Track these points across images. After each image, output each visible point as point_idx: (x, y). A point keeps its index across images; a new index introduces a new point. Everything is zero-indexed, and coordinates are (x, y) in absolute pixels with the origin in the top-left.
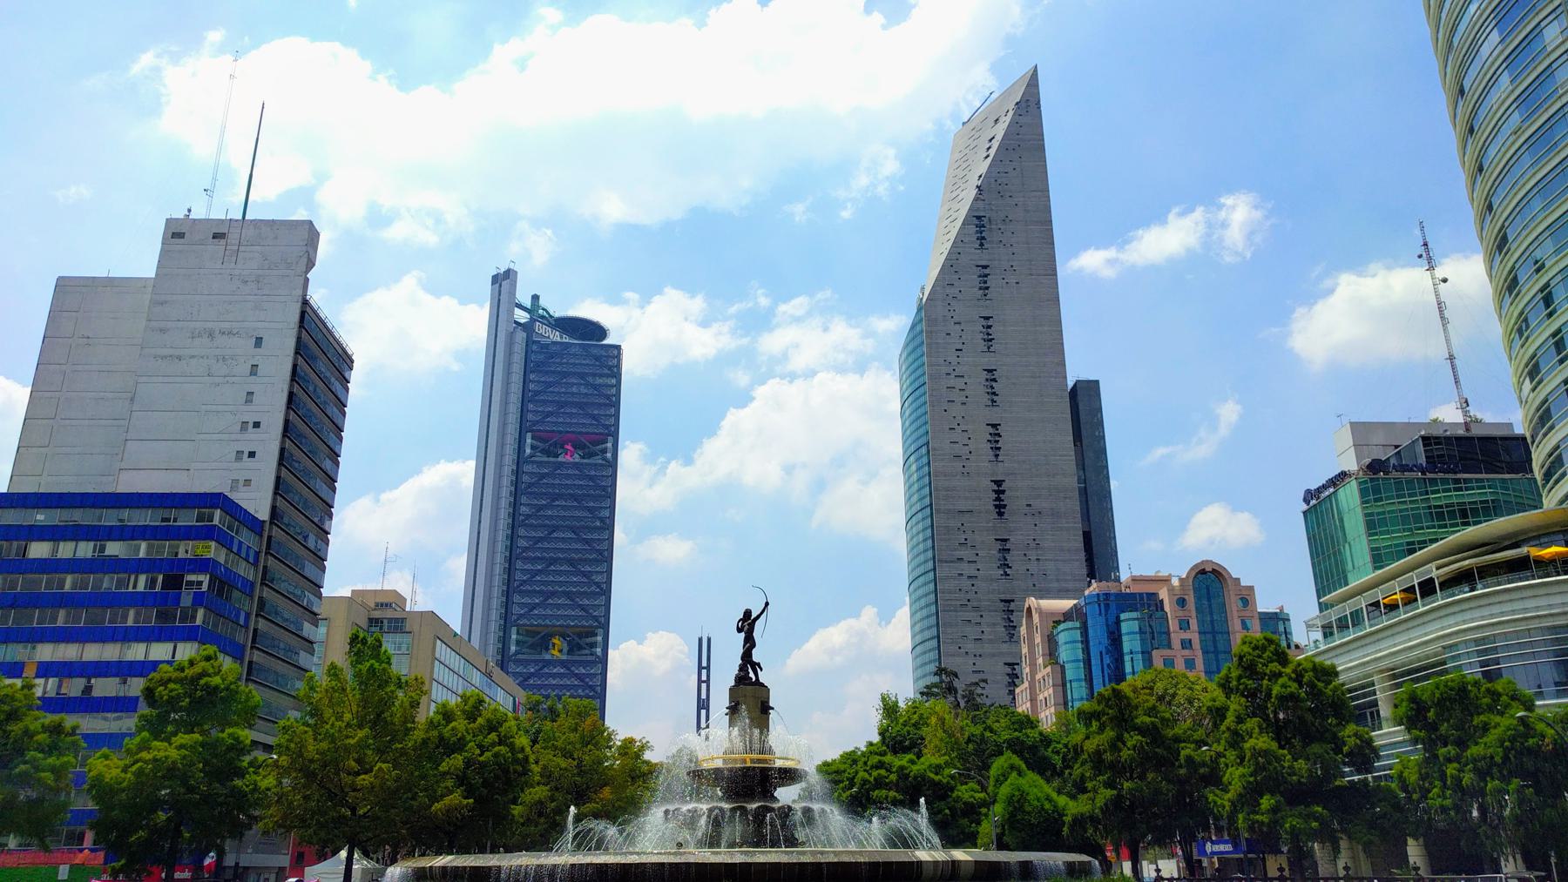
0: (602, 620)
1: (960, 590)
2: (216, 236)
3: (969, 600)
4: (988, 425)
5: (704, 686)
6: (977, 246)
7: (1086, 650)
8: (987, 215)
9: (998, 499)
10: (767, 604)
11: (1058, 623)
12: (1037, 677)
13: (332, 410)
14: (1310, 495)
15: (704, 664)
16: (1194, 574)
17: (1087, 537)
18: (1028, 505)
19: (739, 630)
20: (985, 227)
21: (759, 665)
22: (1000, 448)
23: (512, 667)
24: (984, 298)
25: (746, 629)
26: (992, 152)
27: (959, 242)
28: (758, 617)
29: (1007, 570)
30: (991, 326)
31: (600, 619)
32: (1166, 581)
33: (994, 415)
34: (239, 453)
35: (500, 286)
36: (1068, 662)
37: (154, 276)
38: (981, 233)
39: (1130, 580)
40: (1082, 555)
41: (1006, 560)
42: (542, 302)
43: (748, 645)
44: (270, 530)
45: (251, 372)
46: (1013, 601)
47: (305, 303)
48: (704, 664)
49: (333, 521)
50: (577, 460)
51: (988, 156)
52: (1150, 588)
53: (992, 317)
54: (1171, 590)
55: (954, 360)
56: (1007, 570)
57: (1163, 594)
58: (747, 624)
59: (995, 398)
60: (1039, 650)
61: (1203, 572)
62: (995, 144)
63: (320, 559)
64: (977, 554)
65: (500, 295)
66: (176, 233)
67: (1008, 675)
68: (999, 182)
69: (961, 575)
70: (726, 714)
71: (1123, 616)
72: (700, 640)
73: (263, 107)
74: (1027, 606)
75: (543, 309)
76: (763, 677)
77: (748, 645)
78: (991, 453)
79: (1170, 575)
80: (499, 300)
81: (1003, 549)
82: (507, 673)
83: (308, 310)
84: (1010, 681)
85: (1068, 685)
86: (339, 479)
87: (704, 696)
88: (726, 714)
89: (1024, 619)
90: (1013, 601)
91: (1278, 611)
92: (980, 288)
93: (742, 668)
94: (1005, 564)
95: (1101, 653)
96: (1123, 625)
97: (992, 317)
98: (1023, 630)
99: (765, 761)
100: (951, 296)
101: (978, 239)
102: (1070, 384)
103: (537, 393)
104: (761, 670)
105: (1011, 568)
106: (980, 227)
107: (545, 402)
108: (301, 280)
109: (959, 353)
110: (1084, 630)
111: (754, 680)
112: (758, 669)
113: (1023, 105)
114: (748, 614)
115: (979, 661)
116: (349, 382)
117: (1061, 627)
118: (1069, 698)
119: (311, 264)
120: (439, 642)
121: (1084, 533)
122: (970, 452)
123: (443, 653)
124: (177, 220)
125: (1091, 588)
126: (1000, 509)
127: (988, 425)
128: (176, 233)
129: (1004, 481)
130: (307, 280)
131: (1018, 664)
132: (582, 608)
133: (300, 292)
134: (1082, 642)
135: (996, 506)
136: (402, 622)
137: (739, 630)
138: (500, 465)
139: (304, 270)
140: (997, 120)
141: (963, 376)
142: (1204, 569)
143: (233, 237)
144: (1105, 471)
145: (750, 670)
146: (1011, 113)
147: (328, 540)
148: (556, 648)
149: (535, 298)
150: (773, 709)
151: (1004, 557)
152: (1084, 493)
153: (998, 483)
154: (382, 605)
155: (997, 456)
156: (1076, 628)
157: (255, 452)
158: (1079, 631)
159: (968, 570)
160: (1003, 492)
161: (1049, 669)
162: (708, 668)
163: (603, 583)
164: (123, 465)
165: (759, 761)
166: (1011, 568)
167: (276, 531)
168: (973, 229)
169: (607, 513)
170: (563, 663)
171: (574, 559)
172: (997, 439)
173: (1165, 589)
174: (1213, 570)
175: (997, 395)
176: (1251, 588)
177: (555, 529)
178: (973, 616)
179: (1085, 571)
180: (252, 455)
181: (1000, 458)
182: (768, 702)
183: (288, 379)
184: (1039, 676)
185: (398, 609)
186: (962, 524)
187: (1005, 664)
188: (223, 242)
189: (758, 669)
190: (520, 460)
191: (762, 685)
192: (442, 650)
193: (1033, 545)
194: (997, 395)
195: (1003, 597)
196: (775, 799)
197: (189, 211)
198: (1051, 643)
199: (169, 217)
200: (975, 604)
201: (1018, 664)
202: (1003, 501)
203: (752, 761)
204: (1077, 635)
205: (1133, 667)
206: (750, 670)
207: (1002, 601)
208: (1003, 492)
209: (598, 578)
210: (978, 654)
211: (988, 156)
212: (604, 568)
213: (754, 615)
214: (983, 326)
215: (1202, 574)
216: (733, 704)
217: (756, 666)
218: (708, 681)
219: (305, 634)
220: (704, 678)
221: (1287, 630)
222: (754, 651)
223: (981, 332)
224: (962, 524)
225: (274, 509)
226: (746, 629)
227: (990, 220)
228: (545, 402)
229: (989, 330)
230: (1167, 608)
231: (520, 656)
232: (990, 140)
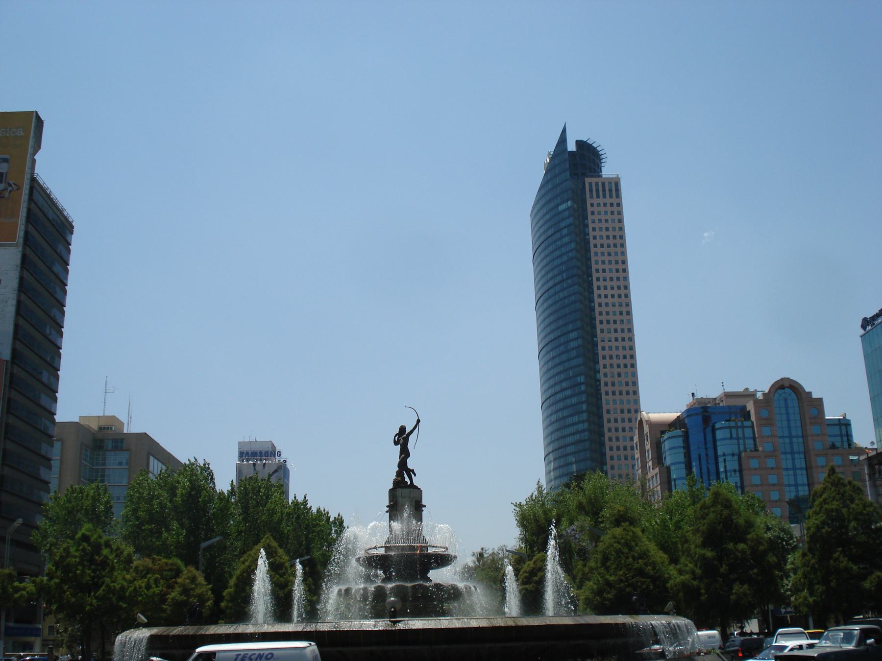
7: (688, 455)
10: (418, 421)
11: (663, 432)
13: (57, 268)
14: (866, 322)
16: (777, 386)
19: (396, 443)
28: (412, 432)
32: (752, 395)
36: (673, 464)
39: (723, 395)
43: (403, 455)
49: (63, 338)
52: (739, 402)
54: (757, 402)
57: (750, 407)
58: (402, 438)
60: (649, 456)
61: (782, 387)
63: (52, 392)
70: (387, 512)
74: (639, 419)
77: (403, 455)
79: (756, 391)
83: (36, 185)
85: (673, 483)
88: (387, 512)
89: (637, 429)
91: (842, 417)
93: (399, 474)
104: (415, 475)
110: (686, 437)
111: (409, 483)
114: (402, 429)
116: (67, 286)
117: (666, 436)
120: (152, 458)
134: (684, 447)
137: (396, 443)
142: (783, 385)
145: (406, 476)
147: (70, 250)
150: (425, 506)
156: (680, 436)
158: (681, 438)
161: (657, 470)
174: (790, 385)
176: (820, 400)
182: (421, 501)
184: (649, 476)
191: (416, 487)
196: (429, 580)
198: (658, 447)
204: (680, 442)
205: (725, 467)
206: (406, 476)
213: (408, 431)
216: (392, 503)
217: (410, 472)
219: (43, 453)
221: (849, 433)
222: (408, 460)
225: (14, 351)
226: (402, 441)
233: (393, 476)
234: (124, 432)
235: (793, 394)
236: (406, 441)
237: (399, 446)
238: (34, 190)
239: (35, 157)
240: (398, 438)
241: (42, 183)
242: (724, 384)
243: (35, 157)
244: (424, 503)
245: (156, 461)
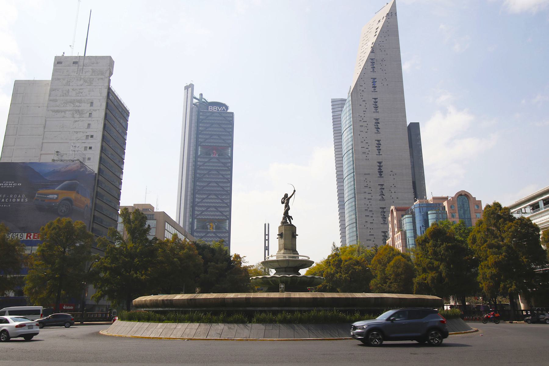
0: (228, 217)
1: (365, 204)
2: (74, 63)
3: (368, 208)
4: (376, 140)
5: (267, 241)
6: (372, 71)
8: (376, 58)
9: (380, 169)
10: (295, 191)
12: (395, 236)
15: (267, 233)
16: (457, 196)
17: (414, 183)
18: (391, 171)
19: (283, 203)
20: (374, 63)
21: (291, 217)
22: (381, 149)
23: (195, 234)
24: (374, 91)
25: (285, 202)
26: (377, 33)
27: (364, 68)
28: (291, 197)
29: (383, 196)
30: (377, 102)
31: (227, 217)
32: (446, 199)
33: (378, 137)
34: (86, 148)
35: (188, 90)
37: (50, 79)
38: (373, 65)
40: (412, 190)
41: (383, 192)
42: (204, 97)
44: (98, 177)
45: (89, 116)
46: (385, 208)
47: (109, 89)
48: (267, 233)
50: (217, 157)
51: (376, 35)
53: (377, 98)
55: (363, 115)
56: (383, 196)
58: (286, 200)
59: (379, 130)
61: (461, 195)
62: (379, 30)
64: (372, 190)
65: (187, 94)
66: (59, 62)
67: (383, 236)
68: (380, 45)
69: (365, 198)
71: (429, 212)
72: (265, 225)
73: (91, 12)
74: (391, 209)
75: (204, 99)
76: (293, 222)
78: (377, 151)
80: (187, 96)
81: (382, 188)
82: (194, 236)
83: (111, 92)
84: (384, 238)
86: (125, 158)
87: (267, 245)
89: (390, 214)
90: (385, 208)
92: (373, 87)
93: (284, 218)
94: (382, 194)
95: (420, 227)
96: (429, 216)
97: (377, 98)
98: (390, 218)
99: (295, 257)
100: (361, 90)
101: (372, 68)
102: (408, 124)
103: (202, 131)
104: (292, 219)
105: (384, 195)
106: (373, 63)
107: (205, 134)
108: (107, 80)
109: (364, 112)
111: (289, 223)
112: (291, 219)
113: (390, 14)
114: (286, 195)
115: (372, 231)
118: (408, 244)
119: (111, 74)
120: (167, 223)
121: (413, 182)
122: (369, 151)
123: (168, 227)
124: (59, 57)
125: (416, 202)
126: (380, 172)
127: (376, 140)
128: (59, 62)
129: (382, 162)
130: (110, 80)
131: (387, 232)
132: (221, 199)
133: (107, 84)
135: (379, 172)
136: (153, 216)
137: (283, 203)
138: (188, 159)
139: (109, 75)
140: (379, 21)
141: (366, 122)
142: (461, 194)
143: (81, 63)
144: (421, 158)
145: (287, 219)
146: (385, 18)
148: (211, 227)
149: (201, 95)
151: (382, 191)
152: (413, 167)
153: (380, 163)
154: (145, 210)
155: (379, 152)
157: (90, 158)
159: (369, 196)
160: (382, 166)
162: (268, 235)
163: (229, 190)
164: (42, 152)
165: (293, 257)
166: (384, 195)
167: (101, 178)
168: (370, 64)
169: (229, 189)
170: (214, 233)
171: (217, 181)
172: (379, 146)
173: (446, 201)
175: (380, 129)
177: (210, 194)
178: (370, 214)
179: (413, 196)
180: (90, 148)
181: (381, 153)
183: (104, 118)
184: (396, 236)
185: (151, 211)
186: (366, 179)
187: (382, 232)
188: (77, 65)
189: (291, 219)
190: (196, 157)
192: (168, 226)
193: (393, 186)
194: (380, 129)
195: (381, 206)
197: (64, 53)
199: (56, 56)
200: (371, 209)
201: (387, 232)
202: (382, 170)
203: (290, 257)
204: (411, 220)
206: (287, 219)
207: (380, 208)
208: (382, 166)
209: (226, 201)
210: (372, 230)
211: (376, 35)
212: (229, 185)
214: (374, 102)
215: (460, 196)
217: (290, 218)
218: (268, 240)
219: (114, 218)
220: (267, 236)
222: (289, 211)
223: (373, 104)
224: (366, 179)
225: (100, 169)
226: (285, 202)
227: (377, 61)
228: (205, 134)
229: (376, 103)
230: (447, 209)
231: (198, 230)
232: (377, 29)
233: (281, 219)
234: (155, 211)
235: (466, 198)
236: (288, 203)
237: (284, 205)
238: (110, 94)
239: (110, 78)
240: (284, 200)
241: (120, 99)
242: (432, 193)
243: (110, 78)
244: (297, 233)
245: (169, 225)
